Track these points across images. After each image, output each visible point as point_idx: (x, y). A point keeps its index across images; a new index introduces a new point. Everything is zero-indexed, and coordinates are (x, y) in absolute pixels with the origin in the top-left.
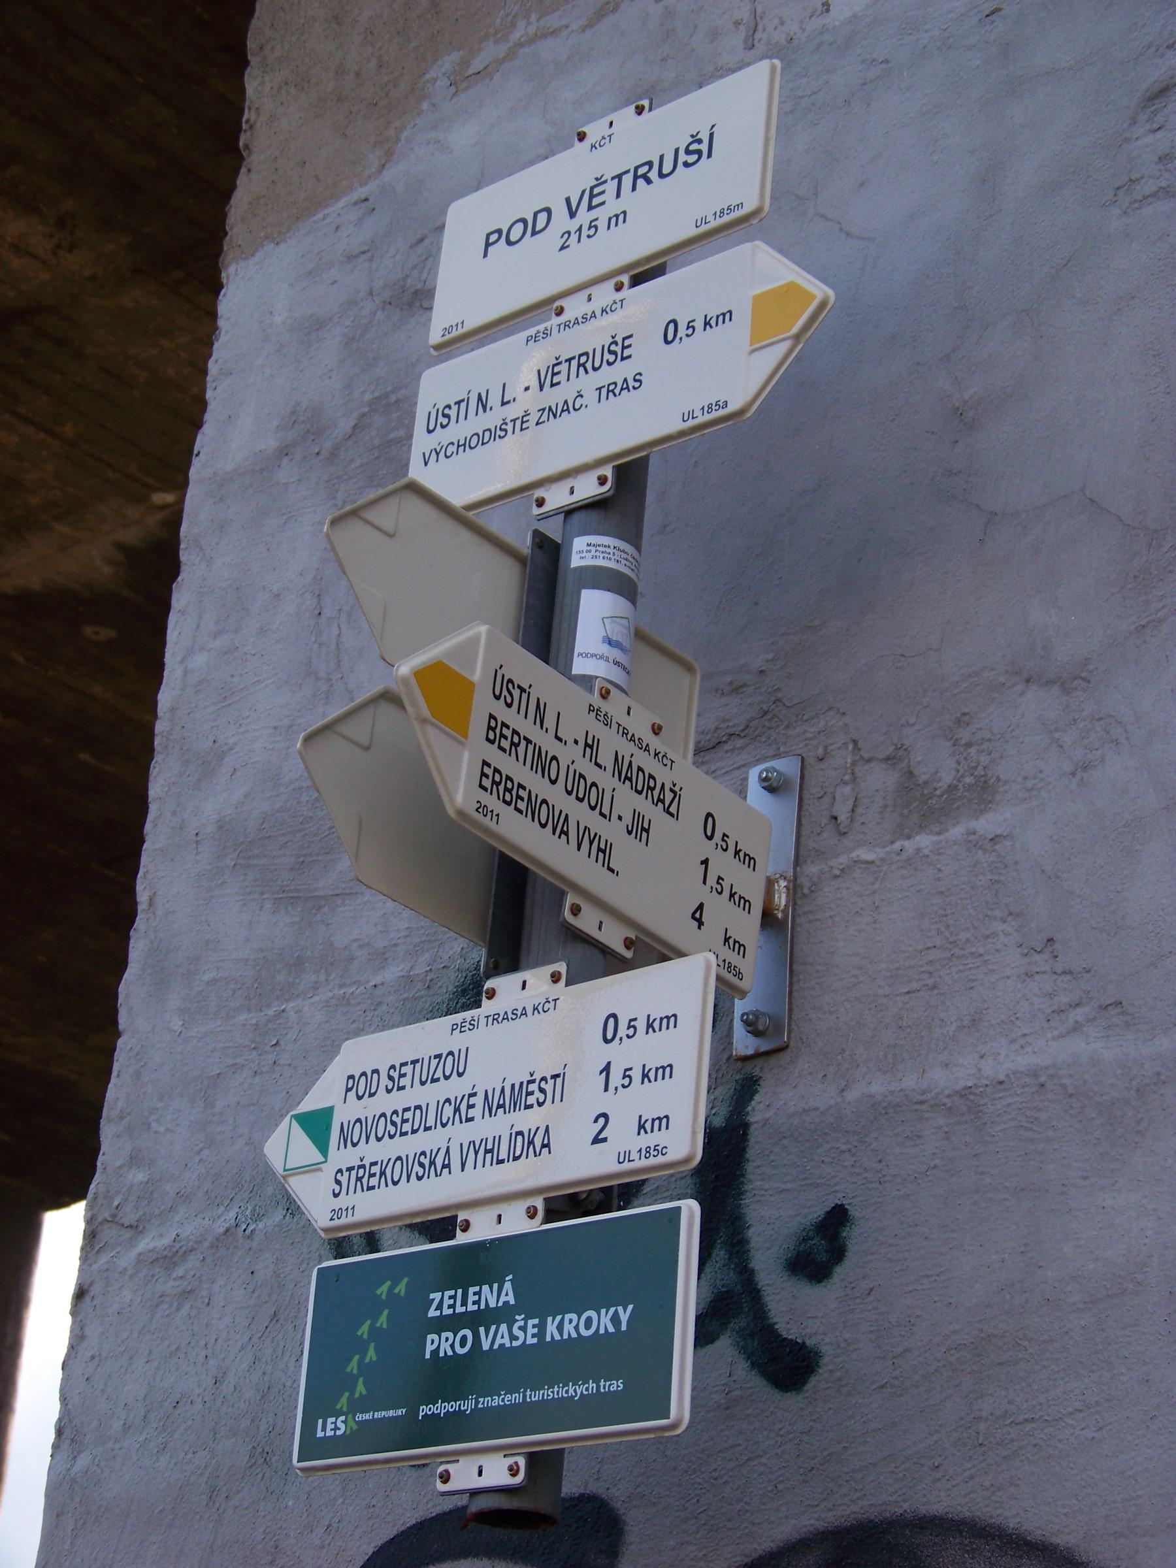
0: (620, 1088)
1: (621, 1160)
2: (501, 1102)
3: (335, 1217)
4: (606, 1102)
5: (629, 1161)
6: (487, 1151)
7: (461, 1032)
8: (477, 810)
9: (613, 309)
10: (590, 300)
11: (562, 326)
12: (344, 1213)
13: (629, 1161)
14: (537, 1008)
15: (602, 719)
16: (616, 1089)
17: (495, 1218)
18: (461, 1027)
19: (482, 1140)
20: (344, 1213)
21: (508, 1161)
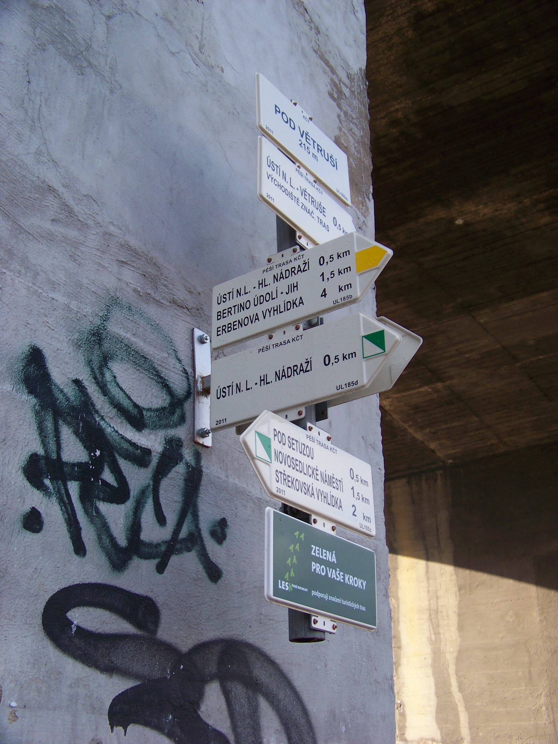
0: (330, 278)
1: (338, 388)
2: (284, 374)
3: (218, 423)
4: (325, 285)
5: (342, 388)
6: (274, 311)
7: (263, 352)
8: (277, 491)
9: (298, 339)
10: (283, 256)
11: (278, 266)
12: (222, 422)
13: (342, 388)
14: (294, 339)
15: (311, 440)
16: (328, 279)
17: (283, 333)
18: (263, 350)
19: (272, 308)
20: (222, 422)
21: (285, 311)
